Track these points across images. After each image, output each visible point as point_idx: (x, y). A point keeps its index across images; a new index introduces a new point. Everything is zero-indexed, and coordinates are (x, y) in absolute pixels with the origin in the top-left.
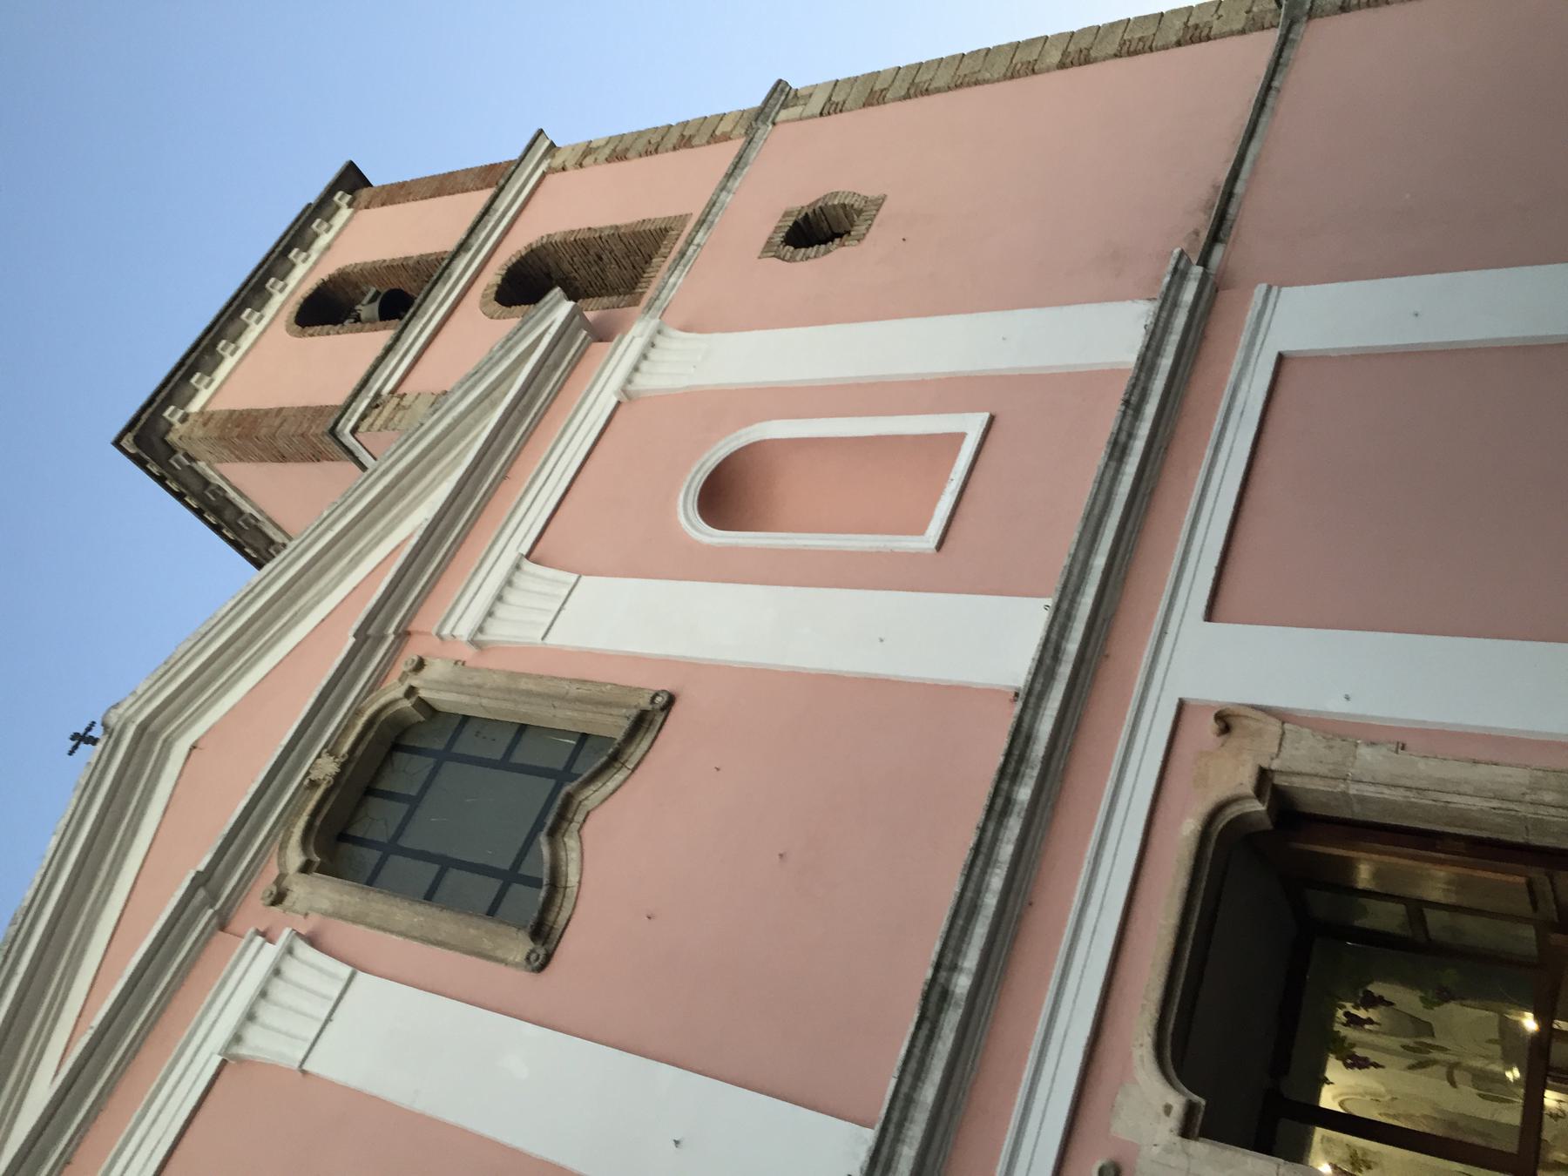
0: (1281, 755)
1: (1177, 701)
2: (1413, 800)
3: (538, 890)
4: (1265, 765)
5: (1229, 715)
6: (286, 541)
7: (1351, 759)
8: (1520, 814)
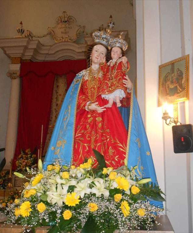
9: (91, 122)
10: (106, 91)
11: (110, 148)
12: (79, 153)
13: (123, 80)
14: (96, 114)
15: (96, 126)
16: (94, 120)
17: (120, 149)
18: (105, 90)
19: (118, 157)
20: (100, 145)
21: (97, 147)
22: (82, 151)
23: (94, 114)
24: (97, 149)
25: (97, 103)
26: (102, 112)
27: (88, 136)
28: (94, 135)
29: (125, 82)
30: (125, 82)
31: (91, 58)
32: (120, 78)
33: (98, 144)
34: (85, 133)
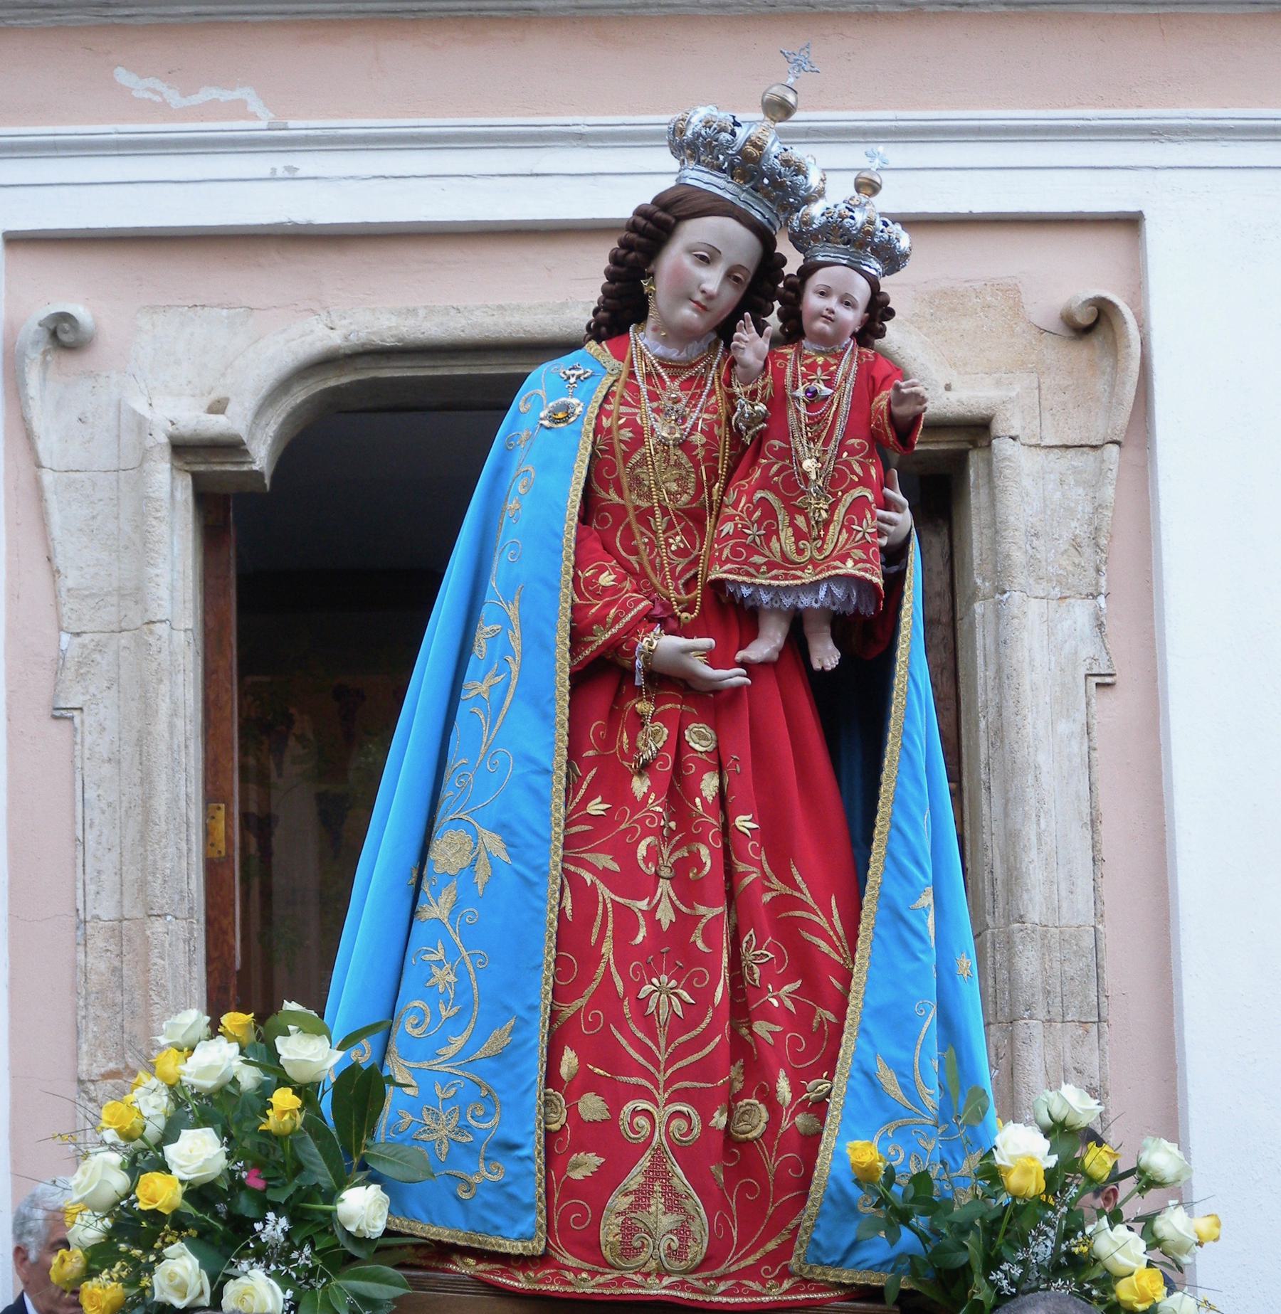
0: (542, 429)
1: (1130, 207)
2: (982, 724)
3: (626, 336)
4: (998, 427)
5: (1111, 325)
6: (569, 853)
7: (1056, 592)
8: (989, 919)
27: (649, 847)
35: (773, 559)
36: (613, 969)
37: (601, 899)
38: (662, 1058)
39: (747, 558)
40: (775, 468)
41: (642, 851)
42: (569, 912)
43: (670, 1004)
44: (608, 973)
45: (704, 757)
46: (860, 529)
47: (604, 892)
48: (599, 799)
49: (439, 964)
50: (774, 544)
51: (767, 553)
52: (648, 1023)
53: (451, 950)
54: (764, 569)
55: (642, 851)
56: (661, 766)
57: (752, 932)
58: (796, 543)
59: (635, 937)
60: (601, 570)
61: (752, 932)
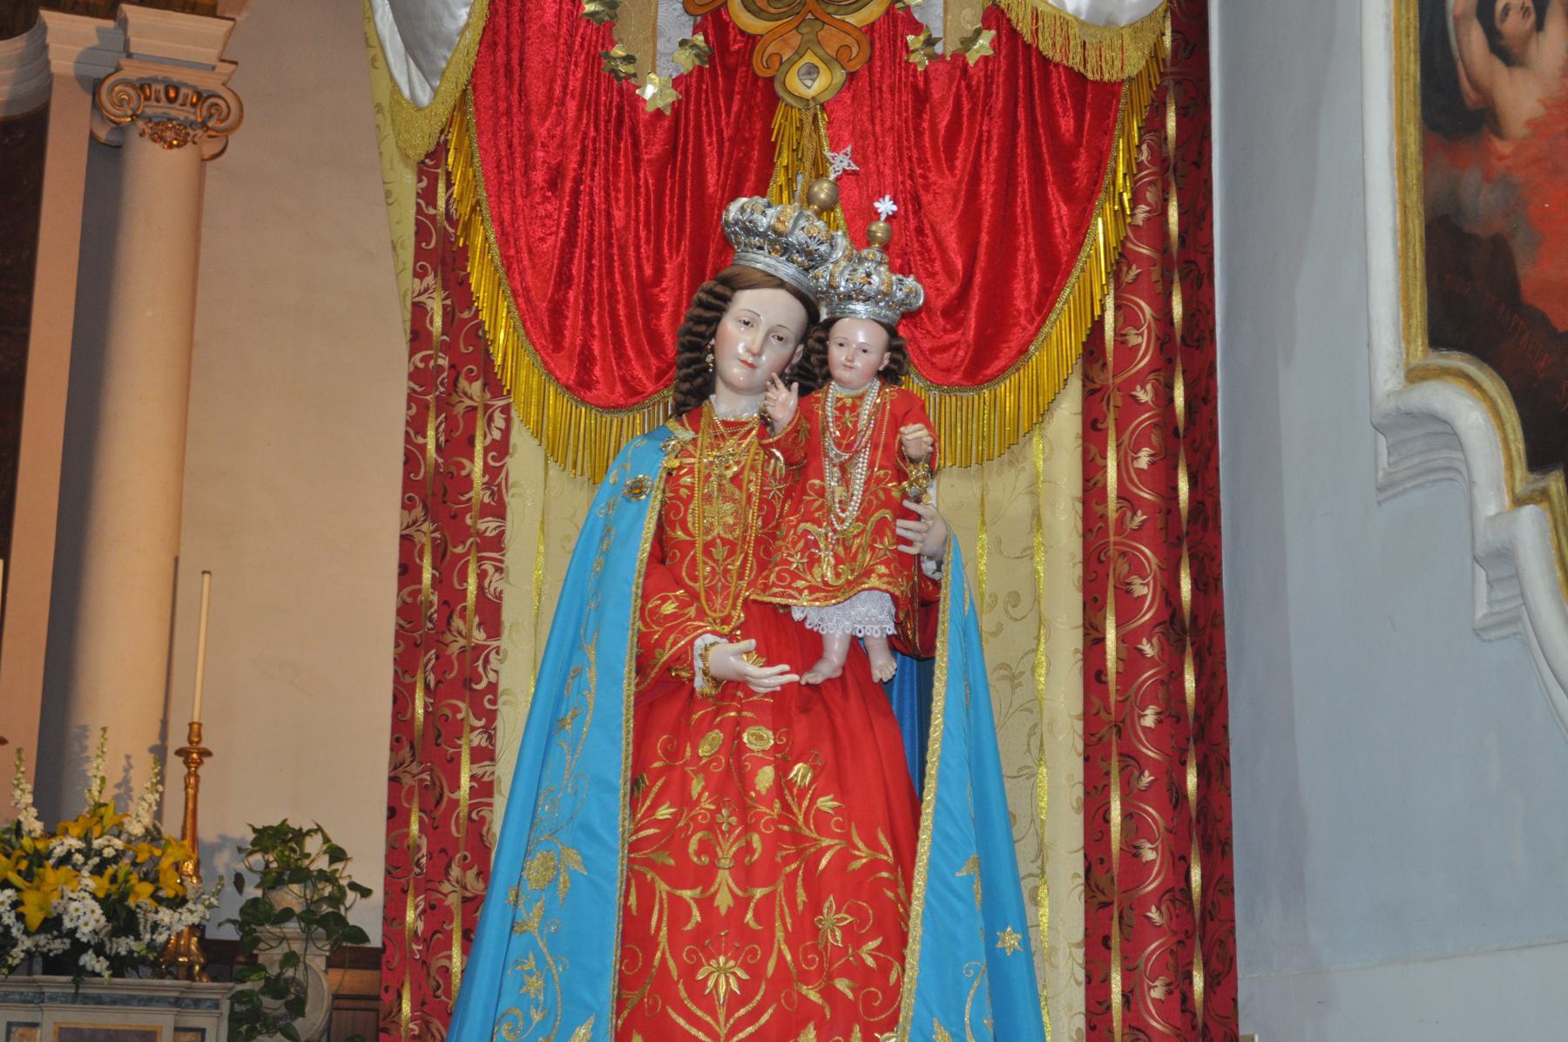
9: (713, 759)
10: (800, 584)
11: (827, 904)
12: (650, 944)
13: (900, 522)
14: (739, 711)
15: (746, 781)
16: (735, 748)
17: (789, 927)
18: (795, 576)
19: (878, 949)
20: (769, 899)
21: (752, 905)
22: (664, 930)
23: (728, 709)
24: (749, 917)
25: (751, 643)
26: (778, 689)
27: (701, 841)
28: (732, 828)
29: (907, 529)
30: (907, 529)
31: (714, 362)
32: (884, 519)
33: (759, 893)
34: (681, 824)
35: (814, 583)
36: (668, 955)
37: (657, 892)
38: (723, 1032)
39: (790, 583)
40: (817, 504)
41: (693, 845)
42: (634, 908)
43: (728, 983)
44: (663, 959)
45: (760, 755)
46: (881, 547)
47: (662, 887)
48: (667, 805)
49: (530, 974)
50: (816, 570)
51: (809, 577)
52: (708, 1004)
53: (540, 959)
54: (806, 592)
55: (693, 845)
56: (715, 767)
57: (831, 898)
58: (836, 566)
59: (686, 924)
60: (665, 600)
61: (831, 898)
